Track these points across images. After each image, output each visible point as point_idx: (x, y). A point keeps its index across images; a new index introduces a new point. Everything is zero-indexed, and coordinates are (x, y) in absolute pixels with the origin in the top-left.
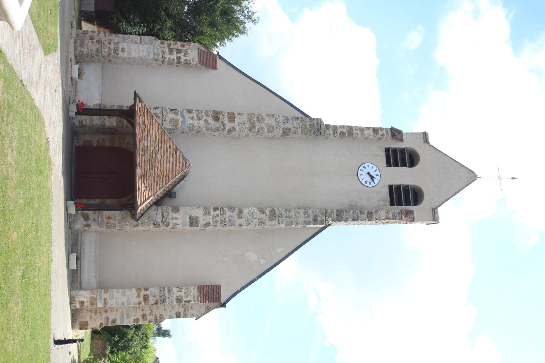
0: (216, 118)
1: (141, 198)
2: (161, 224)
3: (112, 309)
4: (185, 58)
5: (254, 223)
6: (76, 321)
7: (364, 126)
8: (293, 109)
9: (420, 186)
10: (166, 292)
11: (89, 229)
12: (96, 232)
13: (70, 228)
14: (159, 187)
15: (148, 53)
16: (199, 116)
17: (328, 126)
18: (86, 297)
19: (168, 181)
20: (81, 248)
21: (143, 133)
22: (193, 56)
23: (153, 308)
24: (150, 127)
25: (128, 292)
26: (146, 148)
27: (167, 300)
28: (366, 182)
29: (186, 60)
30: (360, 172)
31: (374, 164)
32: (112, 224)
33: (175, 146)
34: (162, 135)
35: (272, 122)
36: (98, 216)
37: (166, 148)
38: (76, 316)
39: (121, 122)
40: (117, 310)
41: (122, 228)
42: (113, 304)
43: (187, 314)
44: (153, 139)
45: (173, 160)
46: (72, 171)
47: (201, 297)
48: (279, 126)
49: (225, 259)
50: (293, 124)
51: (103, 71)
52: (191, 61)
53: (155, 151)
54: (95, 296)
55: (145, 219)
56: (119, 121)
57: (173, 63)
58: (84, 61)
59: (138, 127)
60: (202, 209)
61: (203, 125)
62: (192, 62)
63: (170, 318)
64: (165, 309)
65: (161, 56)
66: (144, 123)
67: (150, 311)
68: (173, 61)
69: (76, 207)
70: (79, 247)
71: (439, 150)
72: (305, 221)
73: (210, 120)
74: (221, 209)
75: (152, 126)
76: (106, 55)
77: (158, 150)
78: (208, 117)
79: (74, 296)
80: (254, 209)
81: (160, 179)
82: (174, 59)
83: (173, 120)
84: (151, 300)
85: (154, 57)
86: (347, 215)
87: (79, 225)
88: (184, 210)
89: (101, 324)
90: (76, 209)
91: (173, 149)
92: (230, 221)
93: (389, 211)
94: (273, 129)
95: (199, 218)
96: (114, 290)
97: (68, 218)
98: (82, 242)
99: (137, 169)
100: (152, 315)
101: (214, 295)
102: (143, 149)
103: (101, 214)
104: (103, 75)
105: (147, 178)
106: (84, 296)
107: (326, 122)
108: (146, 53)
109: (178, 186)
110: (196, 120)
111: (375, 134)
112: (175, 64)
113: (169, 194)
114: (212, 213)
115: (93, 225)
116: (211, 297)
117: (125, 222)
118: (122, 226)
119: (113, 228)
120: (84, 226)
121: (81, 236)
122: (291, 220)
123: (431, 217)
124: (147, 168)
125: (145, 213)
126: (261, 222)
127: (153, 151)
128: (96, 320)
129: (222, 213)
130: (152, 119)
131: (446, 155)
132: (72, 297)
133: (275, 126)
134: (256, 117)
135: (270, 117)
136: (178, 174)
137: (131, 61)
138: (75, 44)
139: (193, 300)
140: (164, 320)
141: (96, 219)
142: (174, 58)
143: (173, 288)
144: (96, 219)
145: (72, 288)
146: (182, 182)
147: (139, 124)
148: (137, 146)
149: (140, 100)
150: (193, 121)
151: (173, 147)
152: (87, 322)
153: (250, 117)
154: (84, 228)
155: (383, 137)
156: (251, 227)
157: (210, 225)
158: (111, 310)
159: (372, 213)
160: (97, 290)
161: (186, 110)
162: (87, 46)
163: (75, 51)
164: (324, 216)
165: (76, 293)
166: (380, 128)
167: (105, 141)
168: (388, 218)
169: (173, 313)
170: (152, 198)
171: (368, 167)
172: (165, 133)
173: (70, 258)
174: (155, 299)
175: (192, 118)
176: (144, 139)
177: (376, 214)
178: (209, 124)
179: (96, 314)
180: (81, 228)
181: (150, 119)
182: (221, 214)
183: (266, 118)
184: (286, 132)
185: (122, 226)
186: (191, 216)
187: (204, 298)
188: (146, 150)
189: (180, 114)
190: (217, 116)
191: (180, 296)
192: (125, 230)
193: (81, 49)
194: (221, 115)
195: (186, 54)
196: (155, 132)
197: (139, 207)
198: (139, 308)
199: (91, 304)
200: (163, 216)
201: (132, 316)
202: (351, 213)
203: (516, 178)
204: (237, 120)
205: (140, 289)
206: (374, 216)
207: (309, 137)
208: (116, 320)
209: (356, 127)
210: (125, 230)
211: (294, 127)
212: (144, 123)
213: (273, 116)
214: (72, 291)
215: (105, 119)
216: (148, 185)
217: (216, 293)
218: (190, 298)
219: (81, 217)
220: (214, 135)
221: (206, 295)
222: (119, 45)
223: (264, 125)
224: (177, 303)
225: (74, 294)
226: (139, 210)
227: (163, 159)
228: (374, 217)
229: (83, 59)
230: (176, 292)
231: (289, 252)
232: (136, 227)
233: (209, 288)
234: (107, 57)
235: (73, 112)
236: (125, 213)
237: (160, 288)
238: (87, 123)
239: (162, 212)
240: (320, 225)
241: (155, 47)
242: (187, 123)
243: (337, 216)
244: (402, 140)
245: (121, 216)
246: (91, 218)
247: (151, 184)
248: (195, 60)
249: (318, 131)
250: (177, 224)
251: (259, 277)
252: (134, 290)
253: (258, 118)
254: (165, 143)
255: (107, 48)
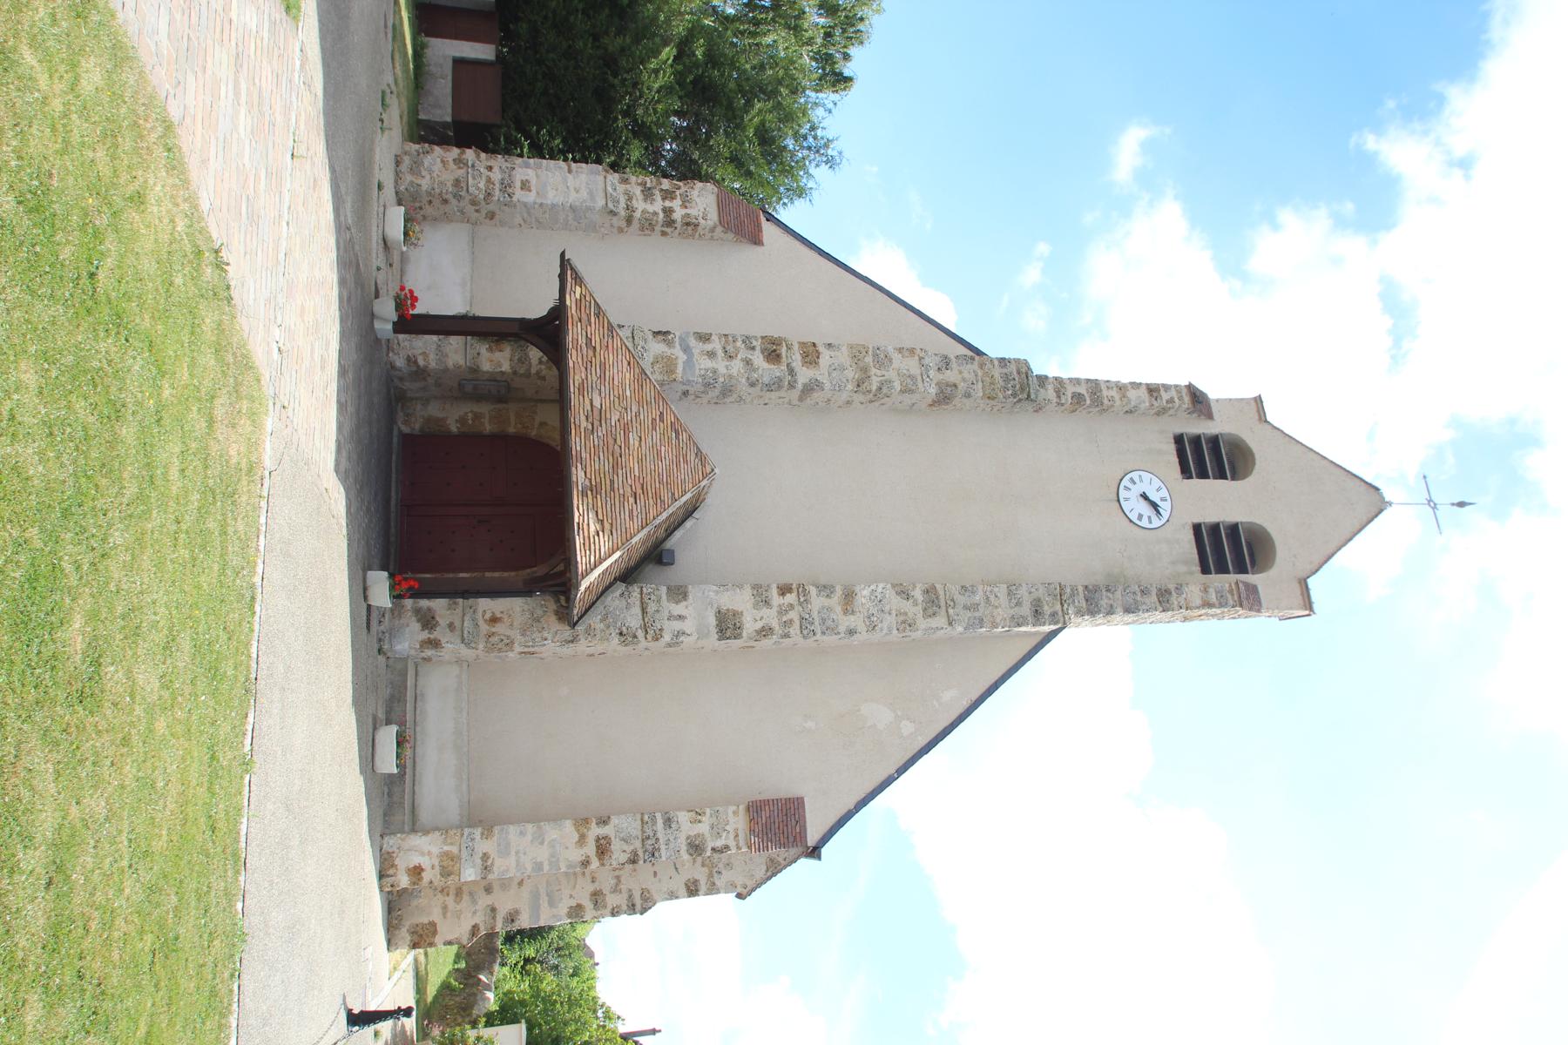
0: (773, 356)
1: (588, 552)
2: (640, 634)
3: (505, 884)
4: (684, 211)
5: (885, 625)
6: (400, 924)
7: (1125, 380)
8: (952, 340)
9: (1264, 525)
10: (658, 824)
11: (439, 654)
12: (459, 662)
13: (380, 651)
14: (636, 524)
15: (591, 193)
16: (728, 348)
17: (1042, 380)
18: (429, 853)
19: (659, 509)
20: (416, 685)
21: (589, 371)
22: (705, 206)
23: (621, 872)
24: (606, 356)
25: (552, 832)
26: (596, 413)
27: (663, 847)
28: (1140, 517)
29: (688, 215)
30: (1123, 494)
31: (1152, 471)
32: (502, 637)
33: (675, 416)
34: (640, 383)
35: (912, 365)
36: (461, 614)
37: (650, 419)
38: (400, 910)
39: (523, 363)
40: (521, 883)
41: (531, 650)
42: (507, 870)
43: (717, 882)
44: (616, 388)
45: (670, 455)
46: (387, 501)
47: (756, 834)
48: (928, 376)
49: (810, 724)
50: (961, 372)
51: (473, 243)
52: (700, 218)
53: (622, 426)
54: (455, 850)
55: (594, 619)
56: (520, 360)
57: (654, 223)
58: (424, 218)
59: (574, 352)
60: (748, 592)
61: (739, 371)
62: (702, 221)
63: (671, 899)
64: (655, 873)
65: (622, 204)
66: (589, 344)
67: (613, 882)
68: (655, 218)
69: (392, 588)
70: (409, 706)
71: (1294, 439)
72: (1013, 617)
73: (758, 359)
74: (800, 590)
75: (611, 355)
76: (482, 196)
77: (629, 423)
78: (751, 352)
79: (393, 852)
80: (883, 588)
81: (638, 501)
82: (655, 214)
83: (663, 359)
84: (619, 853)
85: (607, 204)
86: (1110, 599)
87: (409, 640)
88: (700, 594)
89: (475, 928)
90: (395, 594)
91: (669, 424)
92: (823, 621)
93: (1209, 587)
94: (915, 384)
95: (742, 615)
96: (511, 827)
97: (374, 623)
98: (418, 692)
99: (574, 469)
100: (621, 892)
101: (790, 827)
102: (590, 413)
103: (472, 610)
104: (473, 253)
105: (604, 495)
106: (422, 851)
107: (1037, 369)
108: (584, 194)
109: (678, 534)
110: (720, 359)
111: (1153, 399)
112: (658, 228)
113: (656, 556)
114: (776, 600)
115: (447, 642)
116: (781, 832)
117: (540, 632)
118: (531, 644)
119: (505, 649)
120: (421, 646)
121: (416, 675)
122: (977, 614)
123: (1299, 600)
124: (602, 467)
125: (594, 603)
126: (903, 622)
127: (618, 423)
128: (459, 918)
129: (802, 600)
130: (613, 337)
131: (1311, 450)
132: (386, 856)
133: (919, 378)
134: (870, 353)
135: (907, 354)
136: (686, 493)
137: (548, 216)
138: (397, 166)
139: (734, 843)
140: (655, 904)
141: (457, 624)
142: (657, 211)
143: (678, 813)
144: (456, 624)
145: (387, 828)
146: (689, 524)
147: (575, 342)
148: (572, 404)
149: (578, 280)
150: (714, 362)
151: (669, 418)
152: (433, 925)
153: (857, 353)
154: (422, 652)
155: (1171, 405)
156: (877, 636)
157: (772, 634)
158: (504, 884)
159: (1168, 592)
160: (459, 830)
161: (694, 333)
162: (430, 171)
163: (396, 182)
164: (1059, 603)
165: (400, 841)
166: (1163, 385)
167: (482, 420)
168: (1208, 605)
169: (679, 884)
170: (617, 555)
171: (1141, 481)
172: (648, 380)
173: (377, 741)
174: (629, 848)
175: (711, 355)
176: (590, 385)
177: (1180, 594)
178: (755, 370)
179: (458, 899)
180: (413, 652)
181: (606, 336)
182: (800, 604)
183: (896, 357)
184: (944, 397)
185: (531, 644)
186: (719, 611)
187: (765, 839)
188: (598, 418)
189: (681, 345)
190: (775, 351)
191: (699, 835)
192: (541, 653)
193: (414, 180)
194: (785, 348)
195: (685, 203)
196: (621, 373)
197: (583, 578)
198: (584, 874)
199: (442, 875)
200: (644, 611)
201: (561, 899)
202: (1118, 594)
203: (1470, 504)
204: (825, 359)
205: (586, 821)
206: (1174, 599)
207: (995, 409)
208: (517, 912)
209: (1108, 381)
210: (541, 653)
211: (964, 380)
212: (589, 344)
213: (912, 351)
214: (386, 839)
215: (478, 354)
216: (605, 517)
217: (793, 819)
218: (727, 838)
219: (414, 618)
220: (766, 404)
221: (768, 827)
222: (514, 172)
223: (891, 374)
224: (691, 855)
225: (392, 846)
226: (582, 588)
227: (644, 448)
228: (1176, 603)
229: (421, 208)
230: (686, 826)
231: (974, 699)
232: (571, 645)
233: (776, 806)
234: (483, 203)
235: (385, 320)
236: (540, 604)
237: (642, 814)
238: (430, 361)
239: (641, 601)
240: (1050, 624)
241: (607, 180)
242: (697, 367)
243: (1087, 600)
244: (1210, 416)
245: (528, 615)
246: (443, 622)
247: (614, 514)
248: (709, 215)
249: (1022, 389)
250: (684, 633)
251: (902, 770)
252: (568, 825)
253: (875, 355)
254: (649, 406)
255: (483, 178)
